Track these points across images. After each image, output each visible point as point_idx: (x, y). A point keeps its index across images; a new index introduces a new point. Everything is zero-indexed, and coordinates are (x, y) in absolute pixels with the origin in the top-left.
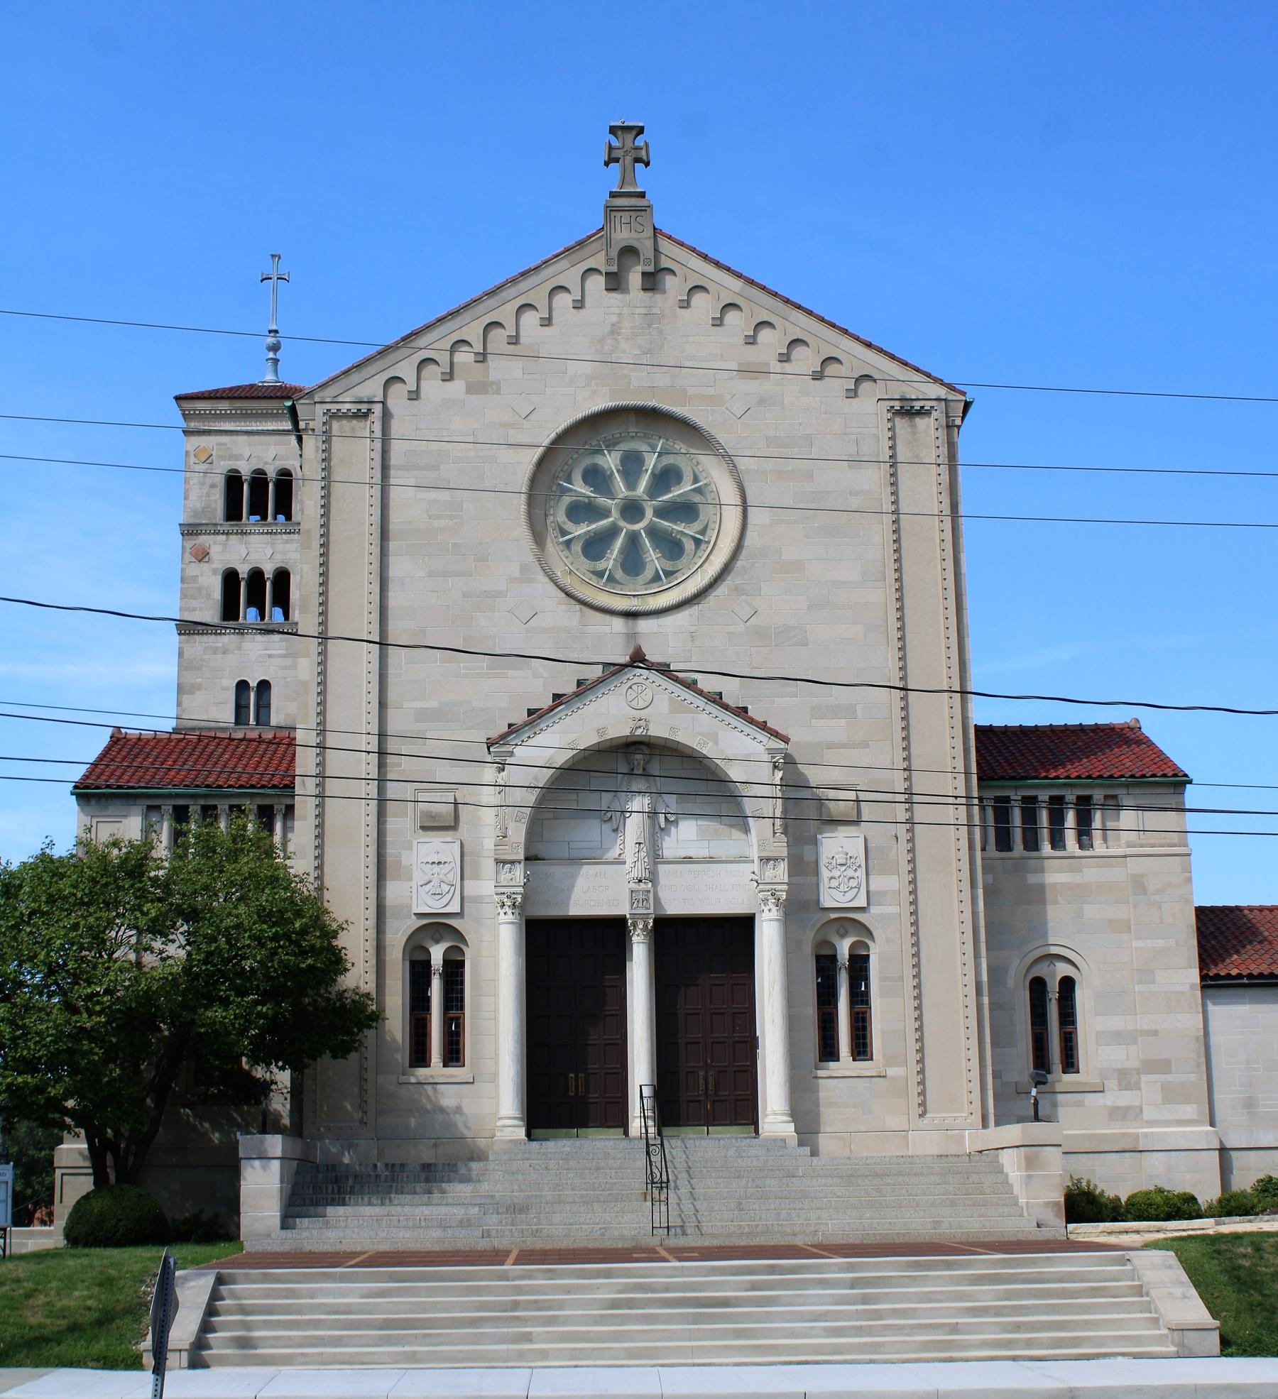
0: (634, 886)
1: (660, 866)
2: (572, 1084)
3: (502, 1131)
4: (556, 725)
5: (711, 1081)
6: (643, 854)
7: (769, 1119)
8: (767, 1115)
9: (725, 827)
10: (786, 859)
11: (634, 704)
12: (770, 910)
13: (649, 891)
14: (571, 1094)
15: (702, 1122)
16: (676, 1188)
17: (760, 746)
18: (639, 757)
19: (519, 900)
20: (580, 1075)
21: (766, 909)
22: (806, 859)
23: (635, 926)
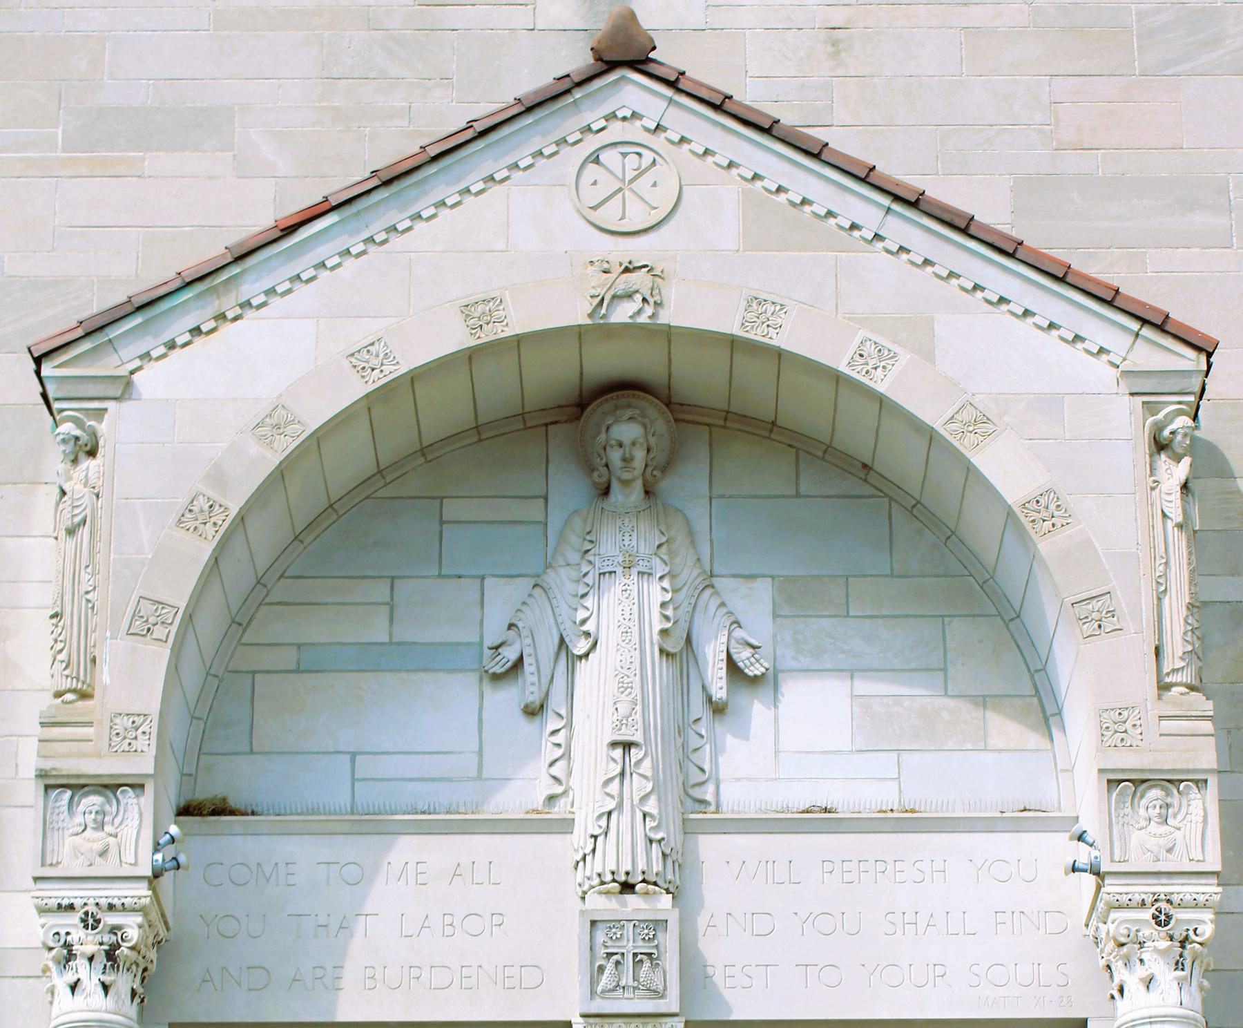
0: (601, 905)
1: (710, 847)
4: (301, 290)
6: (638, 786)
9: (963, 706)
10: (1213, 781)
11: (609, 216)
12: (1149, 982)
17: (1101, 364)
18: (627, 431)
19: (133, 934)
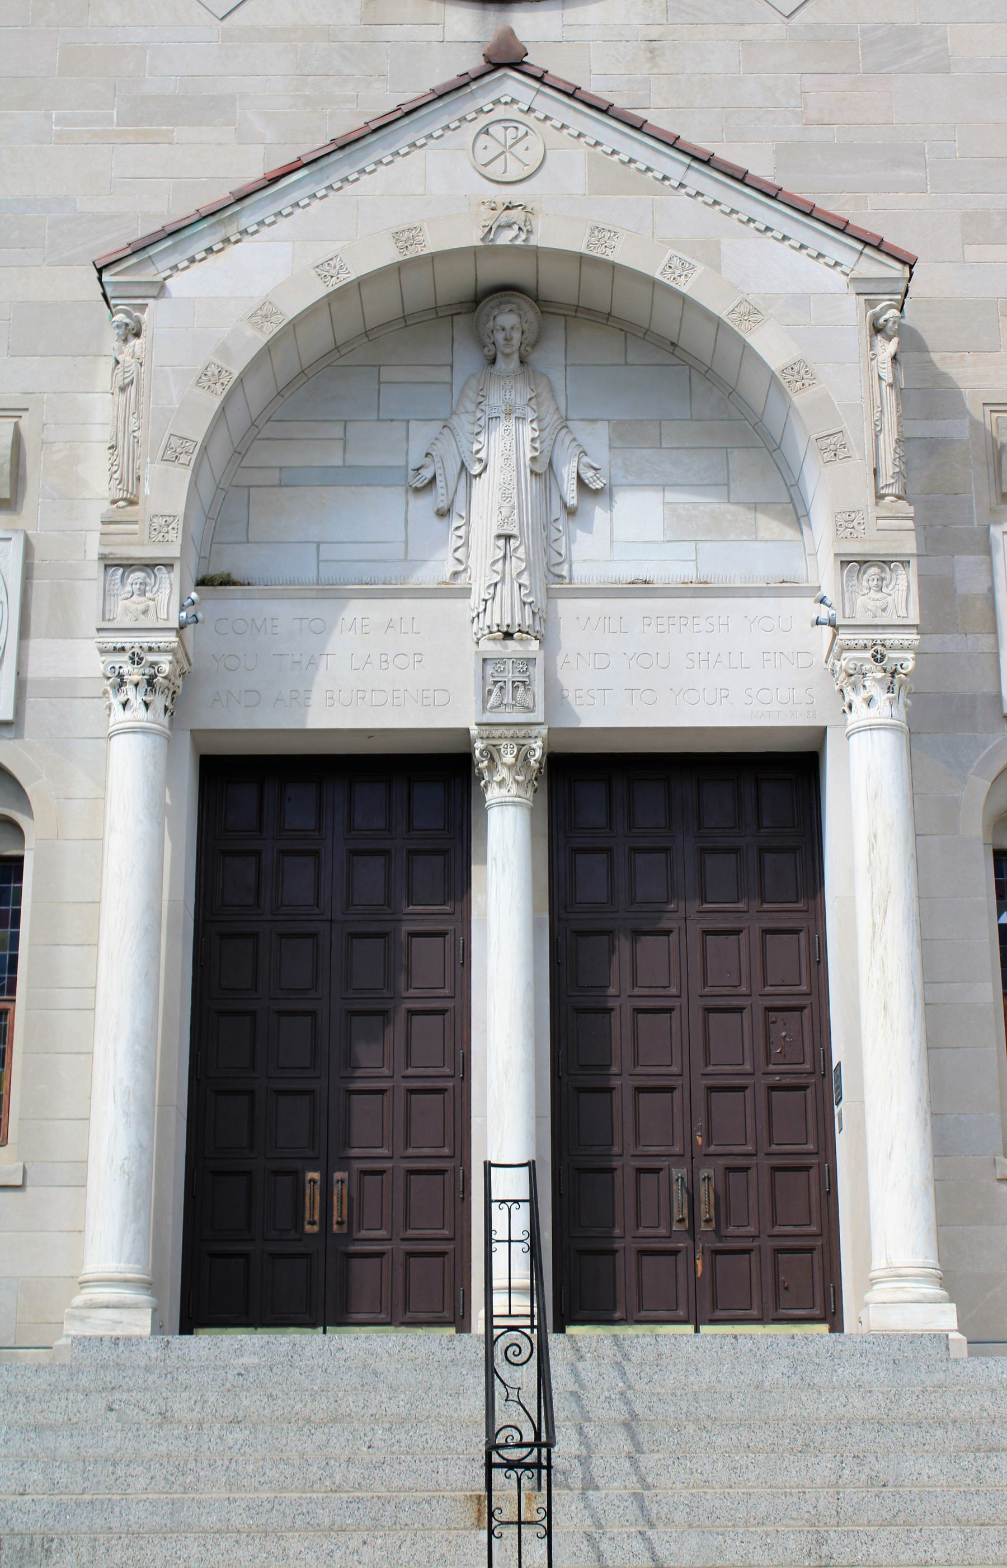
0: (489, 647)
1: (565, 607)
2: (312, 1197)
3: (82, 1319)
4: (282, 222)
5: (705, 1193)
6: (515, 565)
7: (878, 1293)
8: (872, 1282)
10: (914, 562)
11: (495, 170)
12: (869, 701)
13: (531, 661)
14: (308, 1228)
15: (681, 1313)
16: (589, 1484)
17: (836, 273)
19: (166, 668)
20: (338, 1175)
21: (857, 699)
22: (961, 589)
23: (492, 759)
